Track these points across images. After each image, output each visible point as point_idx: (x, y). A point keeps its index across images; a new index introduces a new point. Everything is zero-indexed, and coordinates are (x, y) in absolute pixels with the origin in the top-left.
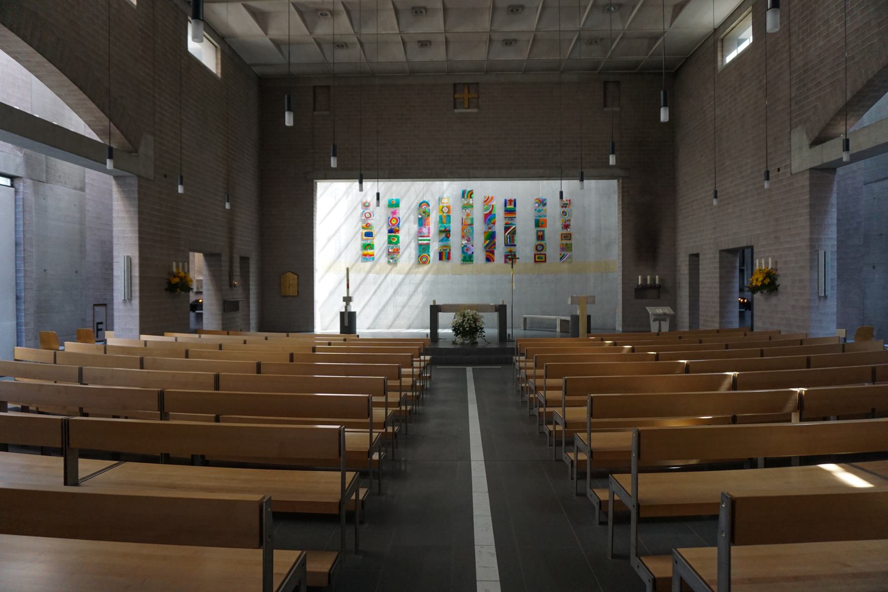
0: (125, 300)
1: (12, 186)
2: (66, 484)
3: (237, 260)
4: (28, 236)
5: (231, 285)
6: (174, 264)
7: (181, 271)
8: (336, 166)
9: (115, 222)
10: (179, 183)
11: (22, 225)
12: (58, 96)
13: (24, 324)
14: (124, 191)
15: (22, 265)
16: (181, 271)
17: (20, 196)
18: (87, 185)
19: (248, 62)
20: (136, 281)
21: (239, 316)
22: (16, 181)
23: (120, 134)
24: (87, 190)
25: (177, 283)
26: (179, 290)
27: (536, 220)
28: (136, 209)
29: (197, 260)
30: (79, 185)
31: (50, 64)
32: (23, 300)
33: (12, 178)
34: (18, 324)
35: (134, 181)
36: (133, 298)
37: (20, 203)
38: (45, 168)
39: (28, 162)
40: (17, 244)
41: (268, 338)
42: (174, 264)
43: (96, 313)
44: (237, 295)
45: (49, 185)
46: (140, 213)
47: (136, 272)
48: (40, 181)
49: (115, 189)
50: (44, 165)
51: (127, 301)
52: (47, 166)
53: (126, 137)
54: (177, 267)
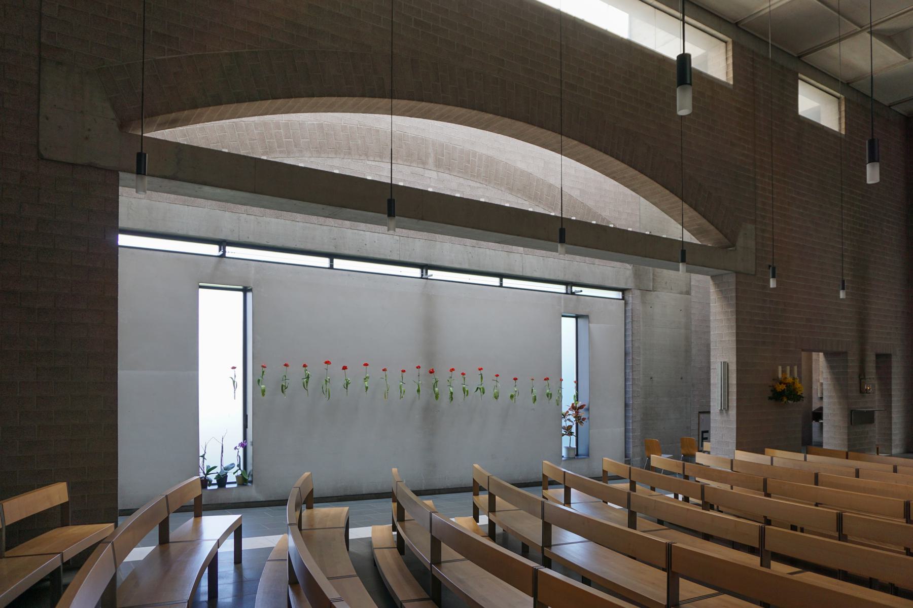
0: (721, 410)
1: (623, 299)
2: (761, 565)
3: (871, 359)
4: (636, 345)
5: (862, 391)
6: (780, 368)
7: (788, 376)
8: (775, 286)
9: (712, 325)
10: (771, 276)
11: (631, 335)
12: (653, 204)
13: (631, 430)
14: (721, 291)
15: (631, 374)
16: (788, 376)
17: (629, 308)
18: (693, 288)
19: (886, 103)
20: (733, 389)
21: (874, 431)
22: (626, 293)
23: (715, 230)
24: (693, 293)
25: (783, 391)
26: (785, 399)
27: (663, 521)
28: (734, 309)
29: (820, 361)
30: (684, 289)
31: (642, 175)
32: (631, 408)
33: (623, 291)
34: (626, 431)
35: (731, 279)
36: (730, 409)
37: (629, 314)
38: (651, 277)
39: (637, 275)
40: (626, 354)
41: (898, 468)
42: (780, 368)
43: (701, 421)
44: (874, 402)
45: (656, 292)
46: (738, 313)
47: (733, 380)
48: (647, 290)
49: (712, 289)
50: (651, 274)
51: (724, 411)
52: (653, 274)
53: (721, 231)
54: (784, 372)
